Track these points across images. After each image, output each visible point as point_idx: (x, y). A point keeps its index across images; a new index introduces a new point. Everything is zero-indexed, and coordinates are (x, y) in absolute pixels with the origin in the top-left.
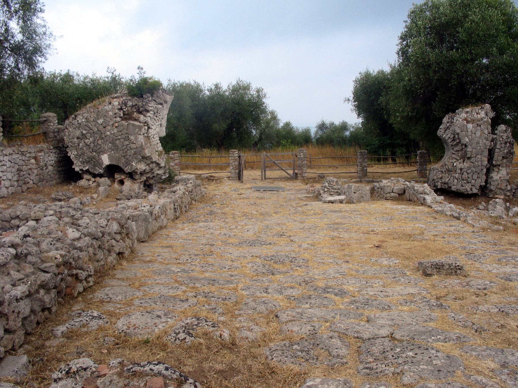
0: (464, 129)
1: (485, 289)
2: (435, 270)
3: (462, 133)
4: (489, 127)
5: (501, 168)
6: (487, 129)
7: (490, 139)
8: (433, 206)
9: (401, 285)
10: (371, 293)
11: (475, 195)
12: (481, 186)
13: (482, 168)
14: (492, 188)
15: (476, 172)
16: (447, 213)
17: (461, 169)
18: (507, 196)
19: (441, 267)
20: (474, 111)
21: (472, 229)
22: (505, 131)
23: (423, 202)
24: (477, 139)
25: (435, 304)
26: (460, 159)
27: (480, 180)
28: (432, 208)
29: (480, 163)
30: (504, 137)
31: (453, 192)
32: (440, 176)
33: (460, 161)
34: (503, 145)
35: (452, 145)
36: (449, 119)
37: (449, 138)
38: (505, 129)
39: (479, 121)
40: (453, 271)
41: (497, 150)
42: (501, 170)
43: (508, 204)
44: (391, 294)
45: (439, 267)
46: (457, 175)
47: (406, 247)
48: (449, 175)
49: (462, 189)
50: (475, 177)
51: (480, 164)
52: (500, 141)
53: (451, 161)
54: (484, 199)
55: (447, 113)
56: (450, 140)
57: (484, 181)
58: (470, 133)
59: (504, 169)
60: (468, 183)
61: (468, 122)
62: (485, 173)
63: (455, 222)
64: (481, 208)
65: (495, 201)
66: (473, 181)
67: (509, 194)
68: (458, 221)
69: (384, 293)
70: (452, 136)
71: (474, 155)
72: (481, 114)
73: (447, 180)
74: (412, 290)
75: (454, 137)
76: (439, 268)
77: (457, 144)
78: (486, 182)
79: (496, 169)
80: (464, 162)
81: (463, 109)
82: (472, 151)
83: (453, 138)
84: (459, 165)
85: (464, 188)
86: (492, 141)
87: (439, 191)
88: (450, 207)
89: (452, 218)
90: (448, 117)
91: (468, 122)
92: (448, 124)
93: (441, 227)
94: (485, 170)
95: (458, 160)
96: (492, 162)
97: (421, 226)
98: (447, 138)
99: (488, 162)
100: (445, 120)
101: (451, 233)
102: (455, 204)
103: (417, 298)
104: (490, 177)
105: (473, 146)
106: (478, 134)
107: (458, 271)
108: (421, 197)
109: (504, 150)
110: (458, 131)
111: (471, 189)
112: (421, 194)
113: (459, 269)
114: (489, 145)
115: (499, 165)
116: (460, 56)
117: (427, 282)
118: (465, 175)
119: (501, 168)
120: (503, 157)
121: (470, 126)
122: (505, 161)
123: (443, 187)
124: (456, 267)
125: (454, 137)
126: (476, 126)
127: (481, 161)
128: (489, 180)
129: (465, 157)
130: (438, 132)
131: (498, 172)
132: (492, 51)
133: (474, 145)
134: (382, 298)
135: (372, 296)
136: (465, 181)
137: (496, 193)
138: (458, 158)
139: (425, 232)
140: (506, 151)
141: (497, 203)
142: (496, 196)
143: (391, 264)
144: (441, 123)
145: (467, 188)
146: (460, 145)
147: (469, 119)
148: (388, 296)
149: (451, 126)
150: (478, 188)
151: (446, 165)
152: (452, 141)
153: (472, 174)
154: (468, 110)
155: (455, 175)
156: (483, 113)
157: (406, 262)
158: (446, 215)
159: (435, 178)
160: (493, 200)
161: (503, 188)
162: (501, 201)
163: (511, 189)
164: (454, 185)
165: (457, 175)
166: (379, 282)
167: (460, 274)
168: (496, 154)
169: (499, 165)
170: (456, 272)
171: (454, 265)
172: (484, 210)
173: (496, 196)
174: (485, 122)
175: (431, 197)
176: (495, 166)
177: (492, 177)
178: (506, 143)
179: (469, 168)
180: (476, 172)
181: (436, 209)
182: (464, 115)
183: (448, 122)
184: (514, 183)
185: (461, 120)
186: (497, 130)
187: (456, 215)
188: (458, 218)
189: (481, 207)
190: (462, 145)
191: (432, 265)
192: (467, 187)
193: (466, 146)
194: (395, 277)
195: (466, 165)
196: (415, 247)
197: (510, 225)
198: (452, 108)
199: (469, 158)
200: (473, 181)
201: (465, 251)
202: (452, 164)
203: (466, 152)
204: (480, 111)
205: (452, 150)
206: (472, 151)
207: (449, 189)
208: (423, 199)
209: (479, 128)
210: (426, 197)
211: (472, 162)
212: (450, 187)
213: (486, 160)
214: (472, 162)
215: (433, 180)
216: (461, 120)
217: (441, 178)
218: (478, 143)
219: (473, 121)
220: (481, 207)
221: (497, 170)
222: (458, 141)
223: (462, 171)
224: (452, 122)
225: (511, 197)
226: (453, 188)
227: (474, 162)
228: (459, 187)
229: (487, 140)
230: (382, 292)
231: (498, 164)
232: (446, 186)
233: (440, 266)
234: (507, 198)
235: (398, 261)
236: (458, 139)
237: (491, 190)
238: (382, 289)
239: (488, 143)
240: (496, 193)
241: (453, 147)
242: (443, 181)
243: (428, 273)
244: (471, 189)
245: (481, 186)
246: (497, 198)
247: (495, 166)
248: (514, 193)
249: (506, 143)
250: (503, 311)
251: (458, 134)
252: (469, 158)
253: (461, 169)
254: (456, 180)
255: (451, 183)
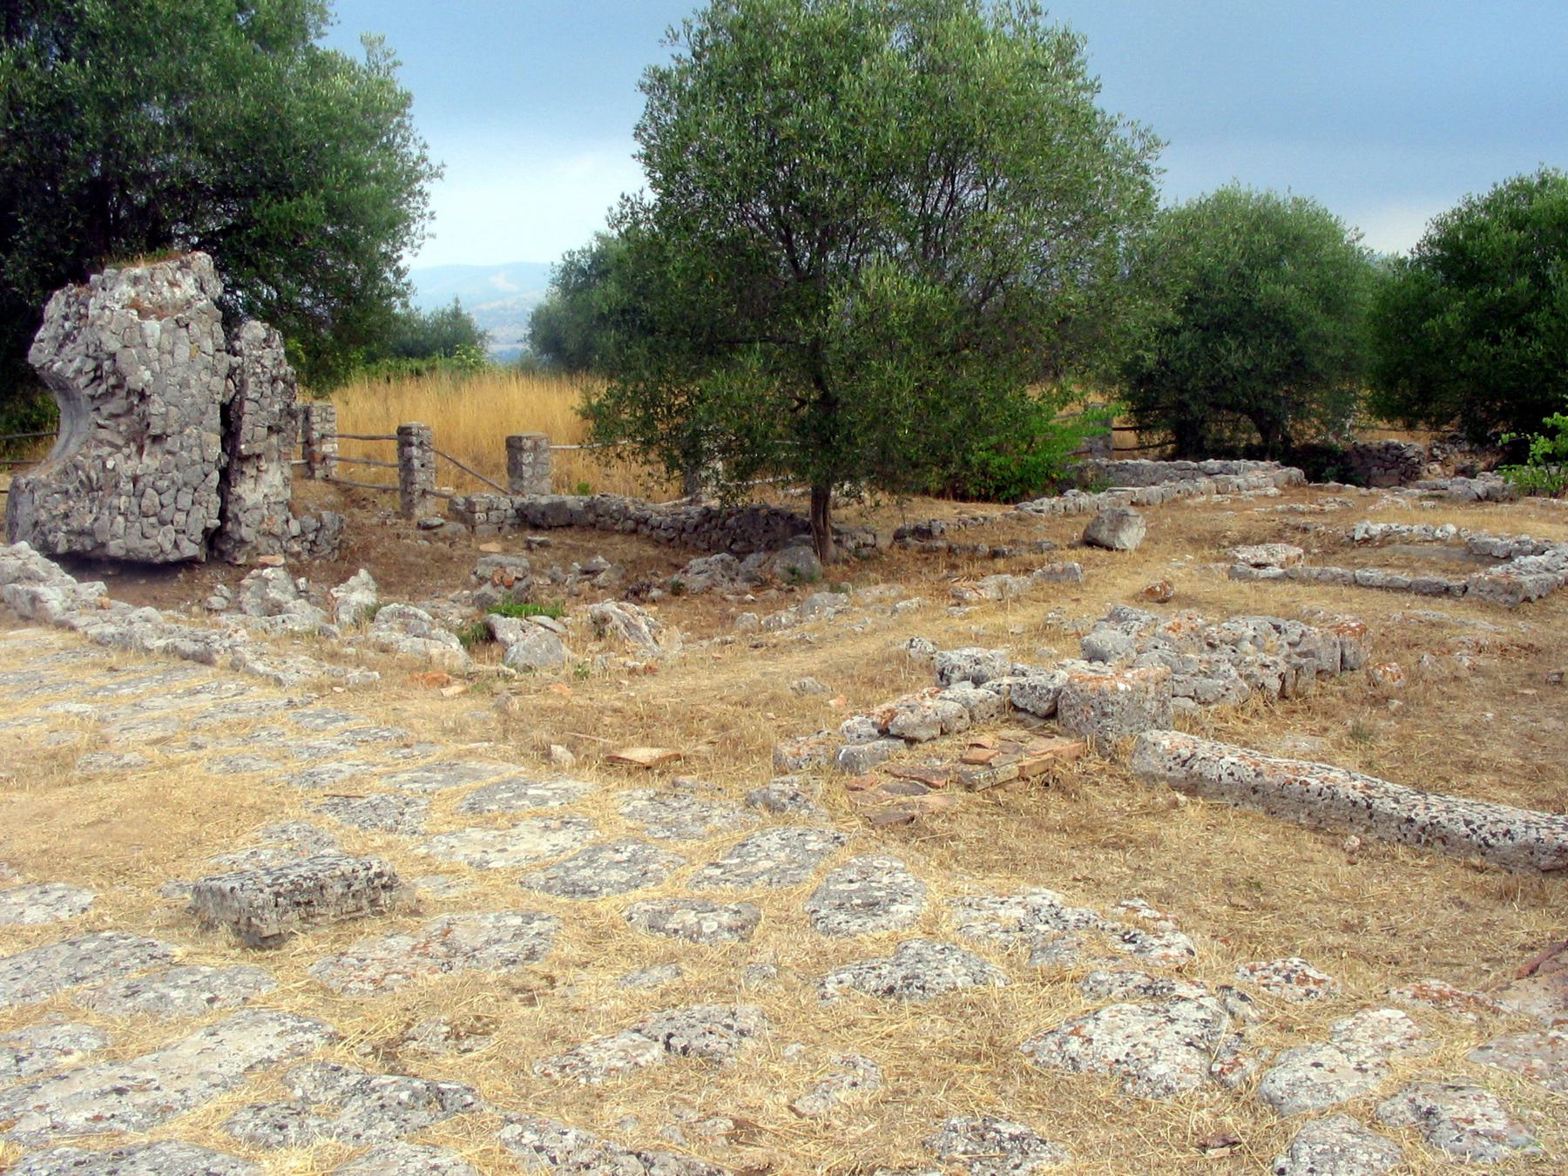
0: (132, 338)
1: (532, 955)
2: (293, 915)
3: (126, 352)
4: (218, 327)
5: (264, 465)
6: (209, 334)
7: (223, 369)
8: (80, 621)
9: (184, 1022)
10: (77, 1119)
11: (189, 564)
12: (206, 531)
13: (206, 469)
14: (245, 532)
15: (185, 484)
16: (148, 643)
17: (135, 480)
18: (292, 555)
19: (315, 897)
20: (158, 274)
21: (278, 697)
22: (265, 340)
23: (28, 610)
24: (180, 372)
25: (404, 1096)
26: (127, 445)
27: (203, 511)
28: (73, 628)
29: (196, 451)
30: (268, 363)
31: (115, 562)
32: (62, 508)
33: (126, 451)
34: (267, 389)
35: (93, 397)
36: (68, 304)
37: (79, 371)
38: (263, 335)
39: (181, 310)
40: (364, 902)
41: (248, 406)
42: (266, 471)
43: (303, 580)
44: (170, 1094)
45: (305, 899)
46: (123, 502)
47: (83, 819)
48: (93, 501)
49: (144, 549)
50: (185, 500)
51: (196, 456)
52: (255, 374)
53: (94, 453)
54: (220, 573)
55: (60, 284)
56: (82, 381)
57: (215, 512)
58: (153, 353)
59: (273, 467)
60: (163, 523)
61: (143, 314)
62: (215, 484)
63: (200, 676)
64: (216, 606)
65: (259, 576)
66: (180, 518)
67: (296, 548)
68: (209, 670)
69: (141, 1099)
70: (90, 365)
71: (176, 428)
72: (185, 287)
73: (89, 519)
74: (259, 1042)
75: (98, 368)
76: (309, 903)
77: (110, 394)
78: (222, 515)
79: (250, 470)
80: (140, 450)
81: (119, 269)
82: (167, 413)
83: (95, 370)
84: (124, 464)
85: (151, 542)
86: (229, 376)
87: (81, 563)
88: (149, 620)
89: (176, 662)
90: (63, 299)
91: (143, 314)
92: (67, 325)
93: (158, 702)
94: (216, 476)
95: (118, 448)
96: (235, 448)
97: (75, 708)
98: (70, 374)
99: (224, 449)
100: (55, 307)
101: (215, 722)
102: (159, 604)
103: (304, 1084)
104: (231, 498)
105: (168, 395)
106: (183, 353)
107: (384, 898)
108: (16, 592)
109: (270, 405)
110: (113, 345)
111: (176, 545)
112: (17, 580)
113: (384, 887)
114: (221, 389)
115: (259, 457)
116: (92, 83)
117: (278, 981)
118: (151, 500)
119: (264, 465)
120: (270, 428)
121: (153, 326)
122: (274, 439)
123: (77, 547)
124: (370, 880)
125: (98, 368)
126: (172, 325)
127: (200, 446)
128: (233, 508)
129: (144, 437)
130: (33, 351)
131: (256, 479)
132: (201, 72)
133: (172, 392)
134: (141, 1128)
135: (87, 1133)
136: (153, 520)
137: (255, 548)
138: (120, 442)
139: (112, 731)
140: (277, 408)
141: (266, 581)
142: (262, 559)
143: (64, 915)
144: (37, 321)
145: (162, 543)
146: (123, 393)
147: (146, 304)
148: (164, 1111)
149: (79, 329)
150: (199, 537)
151: (76, 468)
152: (93, 380)
153: (172, 491)
154: (137, 271)
155: (115, 502)
156: (188, 279)
157: (125, 893)
158: (148, 651)
159: (44, 516)
160: (255, 572)
161: (277, 530)
162: (281, 573)
163: (303, 533)
164: (114, 537)
165: (123, 502)
166: (75, 1040)
167: (392, 909)
168: (246, 418)
169: (259, 457)
170: (373, 902)
171: (362, 874)
172: (226, 610)
173: (262, 559)
174: (201, 311)
175: (59, 590)
176: (246, 459)
177: (240, 497)
178: (274, 380)
179: (162, 472)
180: (185, 484)
181: (93, 631)
182: (126, 291)
183: (66, 318)
184: (308, 509)
185: (117, 307)
186: (237, 337)
187: (188, 646)
188: (204, 659)
189: (216, 601)
190: (130, 393)
191: (278, 894)
192: (159, 539)
193: (143, 396)
194: (133, 992)
195: (151, 461)
196: (120, 810)
197: (371, 654)
198: (74, 269)
199: (156, 439)
200: (180, 518)
201: (318, 792)
202: (99, 462)
203: (144, 417)
204: (178, 275)
205: (93, 415)
206: (167, 413)
207: (98, 552)
208: (26, 598)
209: (183, 332)
210: (40, 589)
211: (169, 452)
212: (103, 545)
213: (214, 440)
214: (169, 452)
215: (36, 524)
216: (117, 307)
217: (66, 516)
218: (184, 384)
219: (160, 311)
220: (216, 601)
221: (254, 472)
222: (112, 381)
223: (140, 485)
224: (82, 317)
225: (305, 556)
226: (115, 548)
227: (176, 449)
228: (135, 542)
229: (215, 373)
230: (120, 1091)
231: (257, 451)
232: (88, 543)
233: (309, 891)
234: (292, 561)
235: (87, 898)
236: (114, 373)
237: (243, 542)
238: (111, 1075)
239: (218, 384)
240: (255, 548)
241: (97, 403)
242: (75, 525)
243: (266, 933)
244: (176, 545)
245: (206, 531)
246: (265, 566)
247: (246, 459)
248: (313, 542)
249: (274, 380)
250: (685, 1050)
251: (112, 356)
252: (156, 439)
253: (135, 480)
254: (120, 519)
255: (103, 532)
